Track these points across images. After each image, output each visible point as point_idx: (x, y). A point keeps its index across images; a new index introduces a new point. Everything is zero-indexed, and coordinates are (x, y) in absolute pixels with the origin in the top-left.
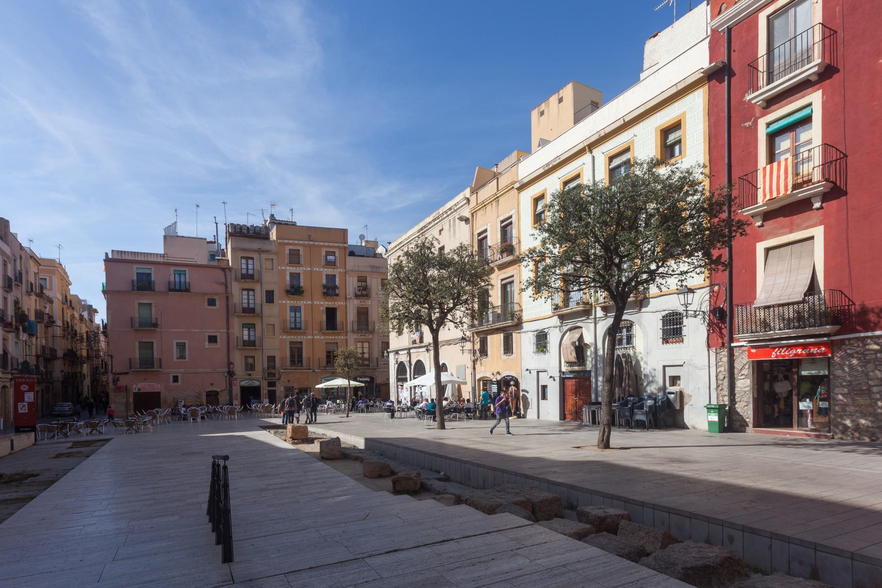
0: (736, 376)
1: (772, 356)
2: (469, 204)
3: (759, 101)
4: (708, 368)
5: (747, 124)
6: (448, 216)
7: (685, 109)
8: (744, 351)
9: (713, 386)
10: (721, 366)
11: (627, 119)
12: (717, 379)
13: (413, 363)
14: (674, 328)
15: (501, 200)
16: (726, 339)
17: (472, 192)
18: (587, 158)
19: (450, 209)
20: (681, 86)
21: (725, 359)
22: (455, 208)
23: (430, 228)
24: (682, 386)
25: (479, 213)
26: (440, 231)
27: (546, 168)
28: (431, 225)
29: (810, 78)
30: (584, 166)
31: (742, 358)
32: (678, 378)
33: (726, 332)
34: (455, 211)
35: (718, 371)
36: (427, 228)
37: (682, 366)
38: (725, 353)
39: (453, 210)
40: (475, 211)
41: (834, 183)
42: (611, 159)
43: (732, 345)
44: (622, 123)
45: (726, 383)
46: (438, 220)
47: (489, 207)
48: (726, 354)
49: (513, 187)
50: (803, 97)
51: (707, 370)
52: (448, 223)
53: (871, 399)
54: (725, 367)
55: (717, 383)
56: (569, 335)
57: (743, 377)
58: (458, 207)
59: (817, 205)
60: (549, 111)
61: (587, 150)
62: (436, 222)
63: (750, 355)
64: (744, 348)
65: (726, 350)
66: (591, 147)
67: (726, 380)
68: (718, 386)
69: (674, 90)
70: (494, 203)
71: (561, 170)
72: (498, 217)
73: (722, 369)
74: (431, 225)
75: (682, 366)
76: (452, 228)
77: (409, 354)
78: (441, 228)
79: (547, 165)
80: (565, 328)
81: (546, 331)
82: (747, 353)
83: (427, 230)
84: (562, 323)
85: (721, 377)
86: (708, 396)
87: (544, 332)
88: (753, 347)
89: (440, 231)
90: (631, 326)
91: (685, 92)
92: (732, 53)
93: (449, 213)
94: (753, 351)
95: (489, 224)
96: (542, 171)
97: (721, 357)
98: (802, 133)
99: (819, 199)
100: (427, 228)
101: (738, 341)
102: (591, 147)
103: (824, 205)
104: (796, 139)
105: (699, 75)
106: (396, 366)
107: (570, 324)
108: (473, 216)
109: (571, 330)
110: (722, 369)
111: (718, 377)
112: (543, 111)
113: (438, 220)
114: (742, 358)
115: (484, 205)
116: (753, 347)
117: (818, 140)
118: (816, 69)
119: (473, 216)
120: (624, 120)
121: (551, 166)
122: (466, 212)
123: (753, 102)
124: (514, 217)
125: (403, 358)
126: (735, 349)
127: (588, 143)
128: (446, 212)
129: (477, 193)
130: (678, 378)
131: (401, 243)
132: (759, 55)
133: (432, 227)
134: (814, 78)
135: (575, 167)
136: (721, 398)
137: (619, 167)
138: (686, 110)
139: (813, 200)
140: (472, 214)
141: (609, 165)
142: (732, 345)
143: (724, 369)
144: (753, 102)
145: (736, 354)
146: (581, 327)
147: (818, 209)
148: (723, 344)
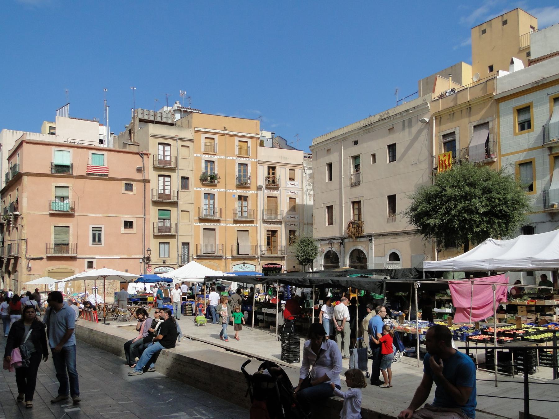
27: (535, 85)
78: (391, 127)
95: (458, 128)
96: (530, 87)
121: (540, 84)
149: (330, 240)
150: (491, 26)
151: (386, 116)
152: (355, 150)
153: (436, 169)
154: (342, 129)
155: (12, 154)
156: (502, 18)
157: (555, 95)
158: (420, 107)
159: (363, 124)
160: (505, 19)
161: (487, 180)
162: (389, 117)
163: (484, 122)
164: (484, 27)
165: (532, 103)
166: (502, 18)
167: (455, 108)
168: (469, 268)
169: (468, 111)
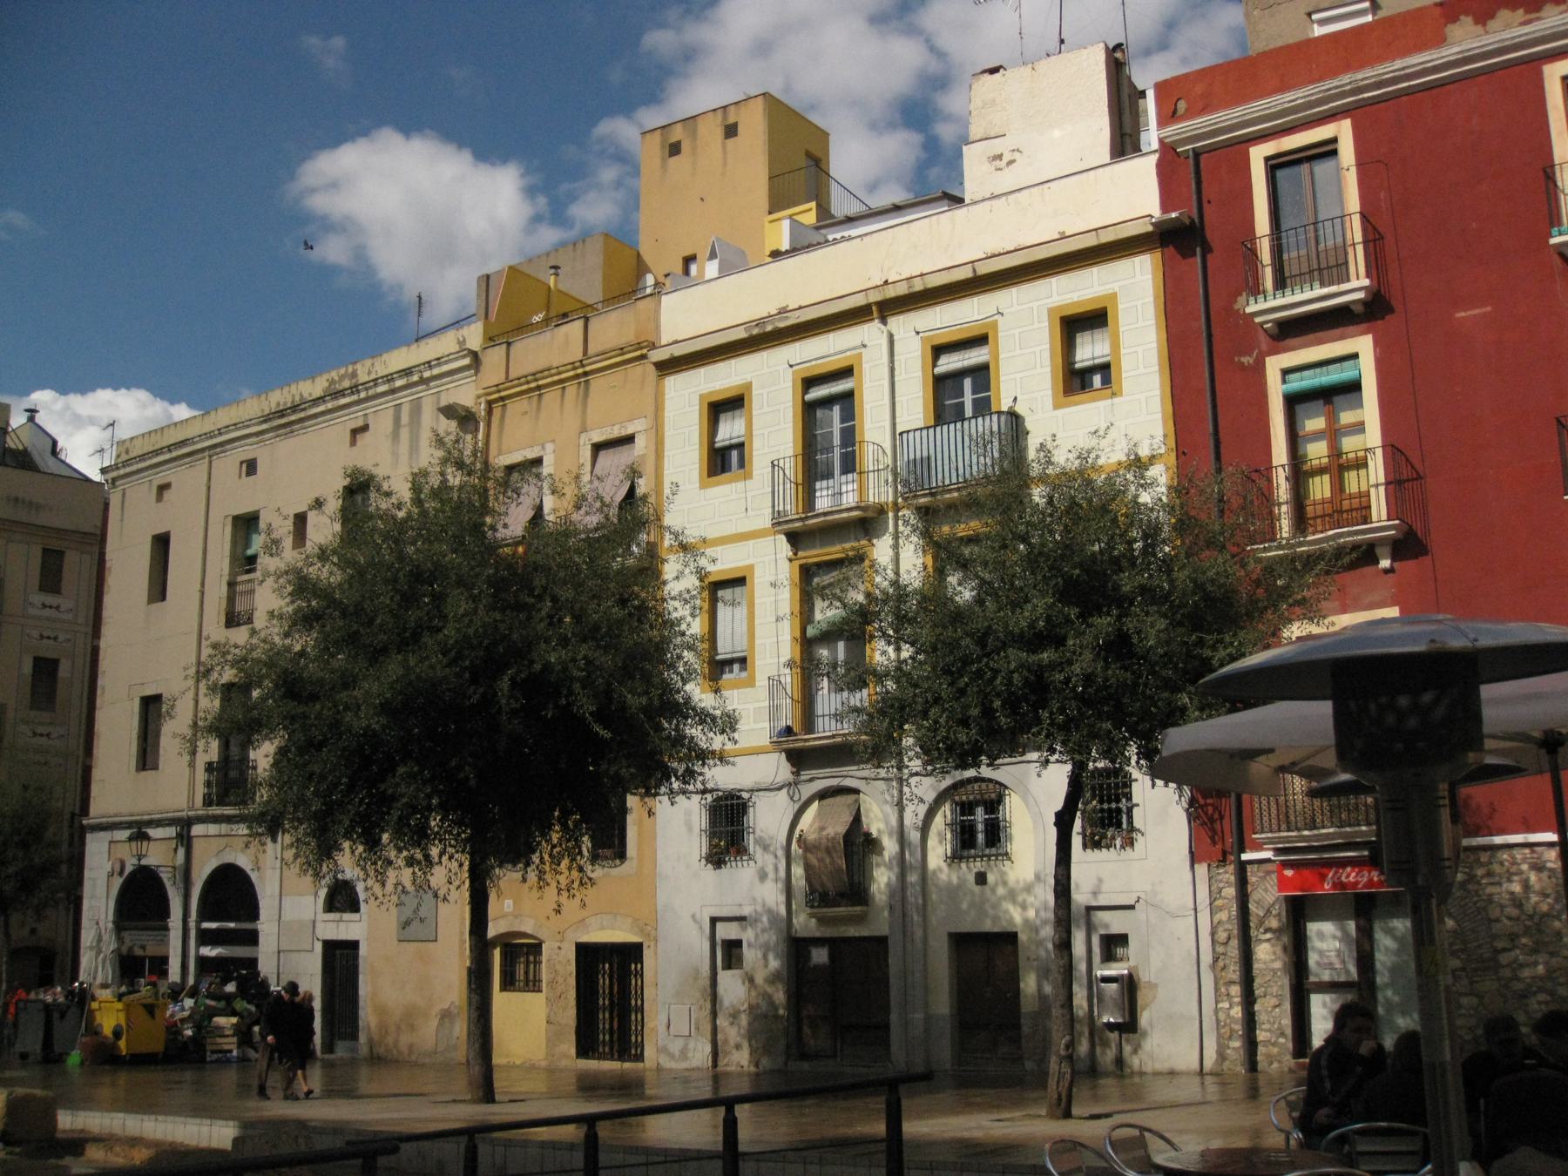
0: (1253, 933)
1: (1326, 887)
2: (477, 372)
3: (1267, 322)
4: (1193, 912)
5: (1246, 360)
6: (393, 391)
7: (1115, 287)
8: (1268, 873)
9: (1207, 958)
10: (1221, 909)
11: (984, 269)
12: (1213, 941)
13: (201, 874)
14: (1109, 803)
15: (597, 383)
16: (1230, 840)
17: (491, 339)
18: (870, 333)
19: (407, 372)
20: (1107, 237)
21: (1230, 892)
22: (427, 374)
23: (315, 416)
24: (1132, 963)
25: (516, 407)
26: (356, 432)
27: (755, 331)
28: (322, 408)
29: (1353, 307)
30: (863, 350)
31: (1266, 890)
32: (1122, 939)
33: (1228, 825)
34: (423, 381)
35: (1216, 920)
36: (302, 415)
37: (1132, 907)
38: (1228, 874)
39: (415, 378)
40: (502, 399)
41: (1411, 527)
42: (938, 351)
43: (1244, 857)
44: (970, 275)
45: (1234, 950)
46: (355, 397)
47: (551, 396)
48: (1232, 878)
49: (643, 357)
50: (1342, 338)
51: (1192, 919)
52: (391, 412)
53: (1499, 979)
54: (1229, 912)
55: (1214, 950)
56: (819, 814)
57: (1268, 936)
58: (436, 371)
59: (1385, 563)
60: (694, 149)
61: (875, 314)
62: (343, 401)
63: (1283, 883)
64: (1269, 867)
65: (1232, 867)
66: (889, 307)
67: (1234, 943)
68: (1216, 960)
69: (1090, 241)
70: (572, 389)
71: (797, 345)
72: (584, 429)
73: (1223, 916)
74: (322, 408)
75: (1132, 907)
76: (405, 434)
77: (185, 840)
78: (360, 423)
79: (760, 322)
80: (808, 790)
81: (745, 795)
82: (1274, 876)
83: (301, 420)
84: (797, 774)
85: (1222, 936)
86: (1196, 985)
87: (739, 797)
88: (1285, 864)
89: (356, 432)
90: (1000, 799)
91: (1067, 264)
92: (1205, 204)
93: (399, 383)
94: (1289, 873)
95: (550, 447)
96: (741, 334)
97: (1221, 885)
98: (1344, 410)
99: (1387, 550)
100: (302, 415)
101: (1258, 847)
102: (889, 307)
103: (1396, 565)
104: (1332, 419)
105: (1145, 227)
106: (118, 882)
107: (824, 779)
108: (490, 412)
109: (823, 795)
110: (1223, 916)
111: (1216, 937)
112: (679, 143)
113: (355, 397)
114: (1266, 890)
115: (535, 386)
116: (1285, 864)
117: (1373, 436)
118: (1361, 295)
119: (490, 412)
120: (974, 271)
121: (769, 328)
122: (466, 394)
123: (1258, 320)
124: (640, 442)
125: (159, 854)
126: (1249, 868)
127: (879, 298)
128: (389, 378)
129: (509, 344)
130: (1122, 939)
131: (183, 443)
132: (1258, 234)
133: (323, 413)
134: (1358, 309)
135: (839, 348)
136: (1223, 990)
137: (959, 375)
138: (1117, 290)
139: (1378, 551)
140: (490, 404)
141: (934, 365)
142: (1244, 857)
143: (1229, 914)
144: (1258, 320)
145: (1252, 879)
146: (856, 791)
147: (1386, 571)
148: (1224, 853)
149: (139, 830)
150: (693, 134)
151: (346, 384)
152: (238, 497)
153: (1013, 672)
154: (213, 413)
155: (93, 726)
156: (725, 117)
157: (808, 368)
158: (446, 362)
159: (278, 404)
160: (731, 120)
161: (23, 502)
162: (354, 389)
163: (623, 433)
164: (677, 134)
165: (749, 386)
166: (725, 117)
167: (543, 378)
168: (116, 816)
169: (581, 392)
